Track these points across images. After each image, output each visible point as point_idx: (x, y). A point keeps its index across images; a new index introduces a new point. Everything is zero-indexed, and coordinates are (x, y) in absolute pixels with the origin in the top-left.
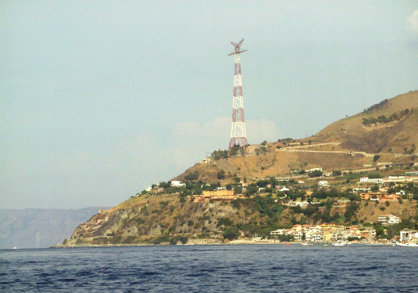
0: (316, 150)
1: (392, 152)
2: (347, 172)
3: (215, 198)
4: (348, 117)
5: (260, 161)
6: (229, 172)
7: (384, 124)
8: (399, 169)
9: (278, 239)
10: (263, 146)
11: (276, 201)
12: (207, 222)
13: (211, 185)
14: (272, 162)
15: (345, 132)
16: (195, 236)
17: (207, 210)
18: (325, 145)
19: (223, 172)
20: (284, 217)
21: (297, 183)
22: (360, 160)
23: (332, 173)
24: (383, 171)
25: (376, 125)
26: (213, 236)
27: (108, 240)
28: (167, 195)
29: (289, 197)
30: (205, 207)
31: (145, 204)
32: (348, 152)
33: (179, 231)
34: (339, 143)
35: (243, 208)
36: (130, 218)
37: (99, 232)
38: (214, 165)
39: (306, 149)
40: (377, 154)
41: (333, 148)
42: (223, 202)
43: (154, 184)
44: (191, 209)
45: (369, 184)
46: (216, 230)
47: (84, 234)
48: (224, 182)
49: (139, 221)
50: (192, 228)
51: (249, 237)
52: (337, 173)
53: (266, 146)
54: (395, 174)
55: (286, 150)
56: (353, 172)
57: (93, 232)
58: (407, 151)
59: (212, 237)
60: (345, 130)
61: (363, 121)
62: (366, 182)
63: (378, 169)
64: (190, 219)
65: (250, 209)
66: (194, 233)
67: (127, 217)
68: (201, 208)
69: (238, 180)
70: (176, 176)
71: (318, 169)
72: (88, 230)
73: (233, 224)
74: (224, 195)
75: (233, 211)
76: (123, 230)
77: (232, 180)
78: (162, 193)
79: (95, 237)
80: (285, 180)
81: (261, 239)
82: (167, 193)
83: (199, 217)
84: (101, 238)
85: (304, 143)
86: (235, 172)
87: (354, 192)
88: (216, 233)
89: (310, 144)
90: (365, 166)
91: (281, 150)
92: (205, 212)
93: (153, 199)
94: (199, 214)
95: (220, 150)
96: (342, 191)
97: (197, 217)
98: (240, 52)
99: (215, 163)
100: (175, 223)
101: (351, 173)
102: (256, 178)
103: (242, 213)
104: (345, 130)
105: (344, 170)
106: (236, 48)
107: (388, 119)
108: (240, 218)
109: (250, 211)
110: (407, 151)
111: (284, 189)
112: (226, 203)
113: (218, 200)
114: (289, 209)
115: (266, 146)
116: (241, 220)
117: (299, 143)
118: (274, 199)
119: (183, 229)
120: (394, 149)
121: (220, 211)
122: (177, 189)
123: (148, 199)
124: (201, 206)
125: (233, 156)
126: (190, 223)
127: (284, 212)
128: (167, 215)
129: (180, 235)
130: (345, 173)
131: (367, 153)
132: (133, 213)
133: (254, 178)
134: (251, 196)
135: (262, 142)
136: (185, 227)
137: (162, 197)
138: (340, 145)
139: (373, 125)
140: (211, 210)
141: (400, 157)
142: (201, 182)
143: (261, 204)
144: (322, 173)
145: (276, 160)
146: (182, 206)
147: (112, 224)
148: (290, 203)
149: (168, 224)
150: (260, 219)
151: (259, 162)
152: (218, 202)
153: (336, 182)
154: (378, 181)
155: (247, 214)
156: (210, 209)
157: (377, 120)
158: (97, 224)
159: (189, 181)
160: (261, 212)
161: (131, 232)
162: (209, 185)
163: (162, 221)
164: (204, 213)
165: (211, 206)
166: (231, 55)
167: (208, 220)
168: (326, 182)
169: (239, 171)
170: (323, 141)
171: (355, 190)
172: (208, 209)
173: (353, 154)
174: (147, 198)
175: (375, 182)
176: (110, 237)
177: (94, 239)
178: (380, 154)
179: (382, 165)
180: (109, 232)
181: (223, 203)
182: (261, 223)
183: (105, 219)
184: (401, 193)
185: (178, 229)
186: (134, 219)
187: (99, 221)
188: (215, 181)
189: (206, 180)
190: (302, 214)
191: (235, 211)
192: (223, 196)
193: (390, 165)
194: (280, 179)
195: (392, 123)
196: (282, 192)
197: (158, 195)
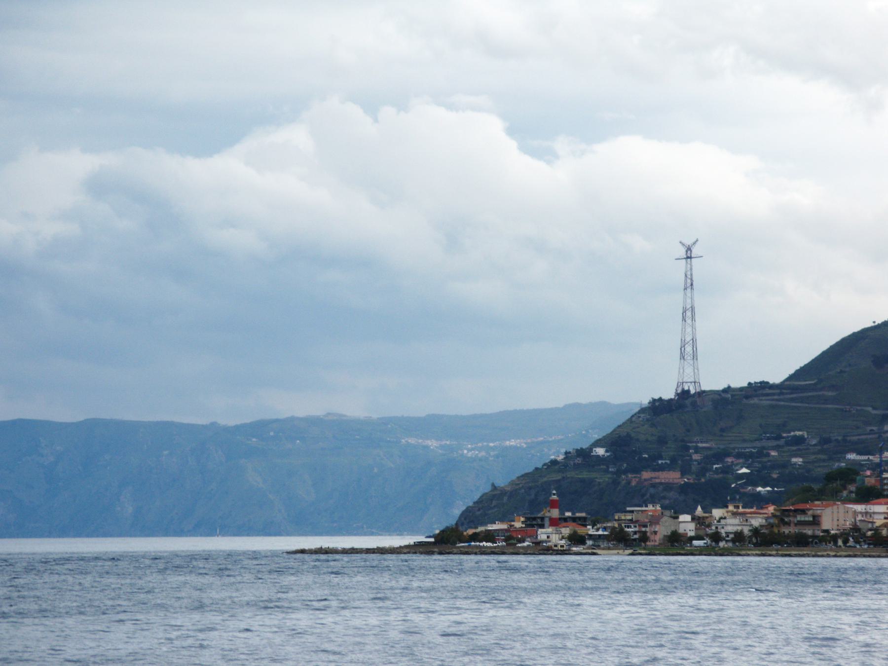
3: (657, 481)
52: (825, 441)
71: (798, 433)
101: (845, 440)
113: (661, 483)
165: (652, 490)
168: (801, 460)
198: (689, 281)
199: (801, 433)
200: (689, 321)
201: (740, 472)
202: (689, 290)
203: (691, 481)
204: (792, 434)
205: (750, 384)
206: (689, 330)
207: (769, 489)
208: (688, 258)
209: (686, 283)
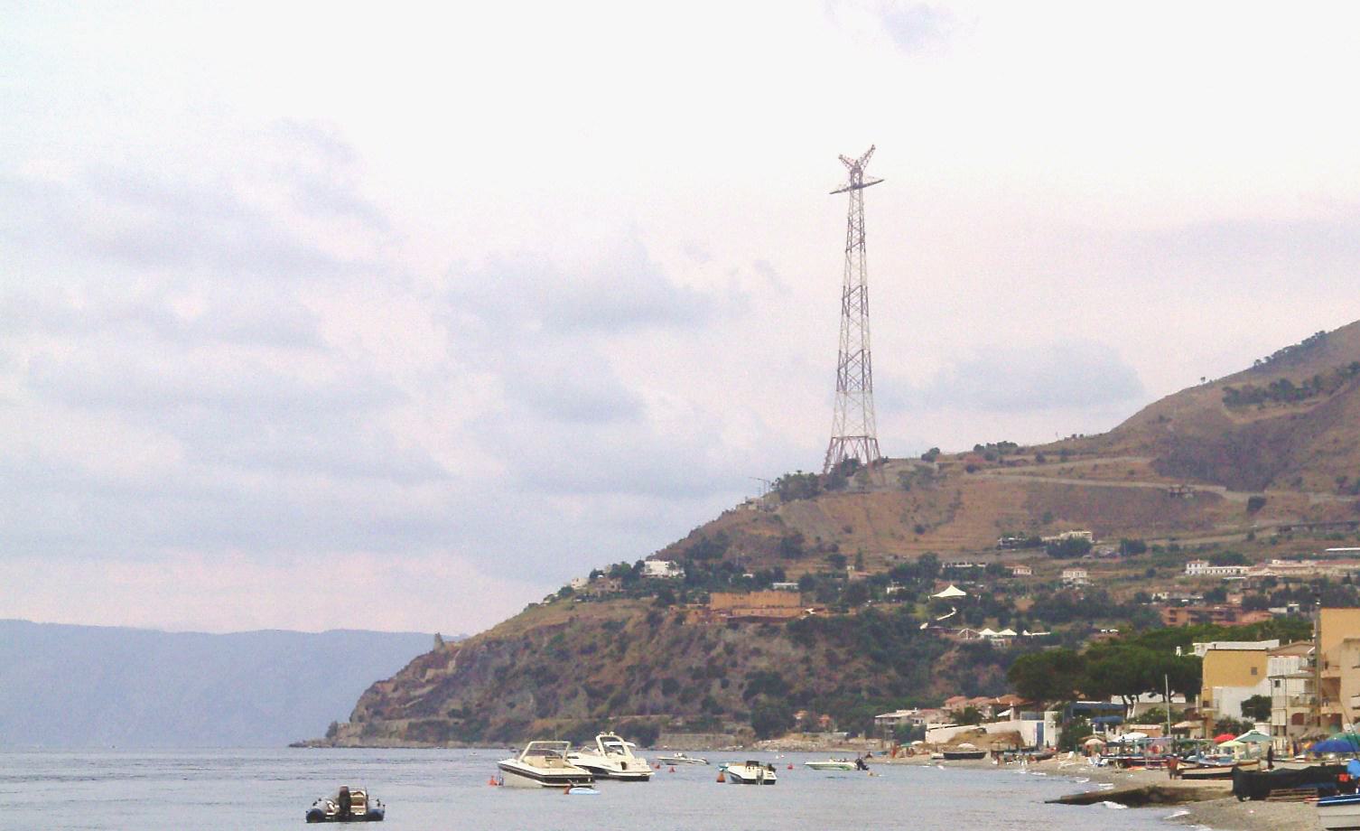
0: (1080, 477)
1: (1303, 487)
2: (1163, 543)
3: (744, 613)
4: (1207, 381)
5: (912, 508)
6: (818, 539)
7: (1285, 406)
8: (1311, 541)
9: (893, 738)
10: (925, 463)
11: (924, 626)
12: (717, 683)
13: (758, 575)
14: (949, 511)
15: (1170, 427)
16: (678, 724)
17: (719, 649)
18: (1106, 466)
19: (798, 538)
20: (941, 673)
21: (1009, 574)
22: (1208, 510)
23: (1119, 546)
24: (1263, 543)
25: (1264, 407)
26: (729, 726)
27: (449, 729)
28: (628, 602)
29: (963, 617)
30: (714, 640)
31: (562, 626)
32: (1174, 486)
33: (635, 708)
34: (1148, 460)
35: (822, 647)
36: (517, 668)
37: (427, 706)
38: (776, 517)
39: (1051, 476)
40: (1259, 495)
41: (1132, 473)
42: (765, 626)
43: (598, 569)
44: (676, 642)
45: (1205, 580)
46: (740, 707)
47: (386, 711)
48: (797, 570)
49: (542, 676)
50: (674, 699)
51: (813, 732)
52: (1132, 548)
53: (935, 466)
54: (1296, 553)
55: (992, 476)
56: (1181, 544)
57: (411, 703)
58: (1346, 485)
59: (726, 727)
60: (1170, 420)
61: (1224, 395)
62: (1203, 575)
63: (1251, 537)
64: (669, 673)
65: (844, 650)
66: (678, 713)
67: (509, 662)
68: (703, 641)
69: (840, 562)
70: (662, 546)
72: (399, 698)
73: (792, 692)
74: (771, 604)
75: (793, 653)
76: (496, 700)
77: (826, 560)
78: (614, 596)
79: (413, 720)
80: (975, 565)
81: (847, 738)
82: (629, 595)
83: (694, 666)
84: (429, 724)
85: (1048, 458)
86: (837, 538)
87: (1155, 603)
88: (739, 717)
89: (1064, 460)
90: (1220, 527)
91: (977, 476)
92: (713, 653)
93: (586, 610)
94: (697, 660)
95: (799, 472)
96: (1120, 602)
97: (690, 669)
98: (865, 186)
99: (779, 512)
100: (628, 685)
101: (1174, 548)
102: (896, 557)
103: (819, 661)
104: (1170, 420)
105: (1153, 539)
106: (852, 173)
107: (1298, 389)
108: (812, 675)
109: (841, 654)
110: (1346, 485)
111: (952, 591)
112: (775, 631)
113: (753, 619)
114: (957, 652)
115: (935, 466)
116: (813, 680)
117: (1032, 458)
118: (919, 622)
119: (649, 703)
120: (1308, 478)
121: (757, 652)
122: (659, 584)
123: (572, 613)
124: (702, 637)
125: (834, 492)
126: (670, 687)
127: (942, 658)
128: (606, 661)
129: (636, 721)
130: (1155, 549)
131: (1230, 489)
132: (528, 652)
133: (890, 558)
134: (850, 610)
135: (925, 450)
136: (656, 696)
137: (613, 608)
138: (1152, 464)
139: (1254, 408)
140: (730, 649)
141: (1326, 505)
142: (729, 567)
143: (876, 632)
144: (1090, 546)
145: (961, 506)
146: (652, 636)
147: (465, 684)
148: (963, 634)
149: (610, 688)
150: (871, 679)
151: (908, 511)
152: (752, 626)
153: (1117, 575)
154: (1238, 571)
155: (832, 660)
156: (727, 645)
157: (1266, 394)
158: (423, 681)
159: (696, 563)
160: (876, 658)
161: (518, 706)
162: (751, 576)
163: (592, 679)
164: (708, 657)
165: (730, 636)
166: (836, 192)
167: (720, 677)
168: (1084, 574)
169: (848, 536)
170: (1104, 453)
171: (1158, 599)
172: (722, 644)
173: (1189, 492)
174: (572, 608)
175: (1229, 576)
176: (456, 720)
177: (411, 726)
178: (1267, 493)
179: (1266, 525)
180: (455, 704)
181: (765, 630)
182: (870, 690)
183: (447, 667)
184: (1288, 611)
185: (634, 702)
186: (526, 671)
187: (430, 673)
188: (767, 565)
189: (748, 559)
190: (994, 667)
191: (800, 653)
192: (768, 607)
193: (1294, 526)
194: (946, 560)
195: (1309, 405)
196: (944, 599)
197: (604, 603)
198: (856, 234)
199: (1080, 534)
200: (855, 314)
201: (942, 595)
202: (856, 251)
203: (826, 615)
204: (1062, 535)
205: (978, 448)
206: (855, 332)
207: (1009, 632)
208: (855, 187)
209: (849, 239)
